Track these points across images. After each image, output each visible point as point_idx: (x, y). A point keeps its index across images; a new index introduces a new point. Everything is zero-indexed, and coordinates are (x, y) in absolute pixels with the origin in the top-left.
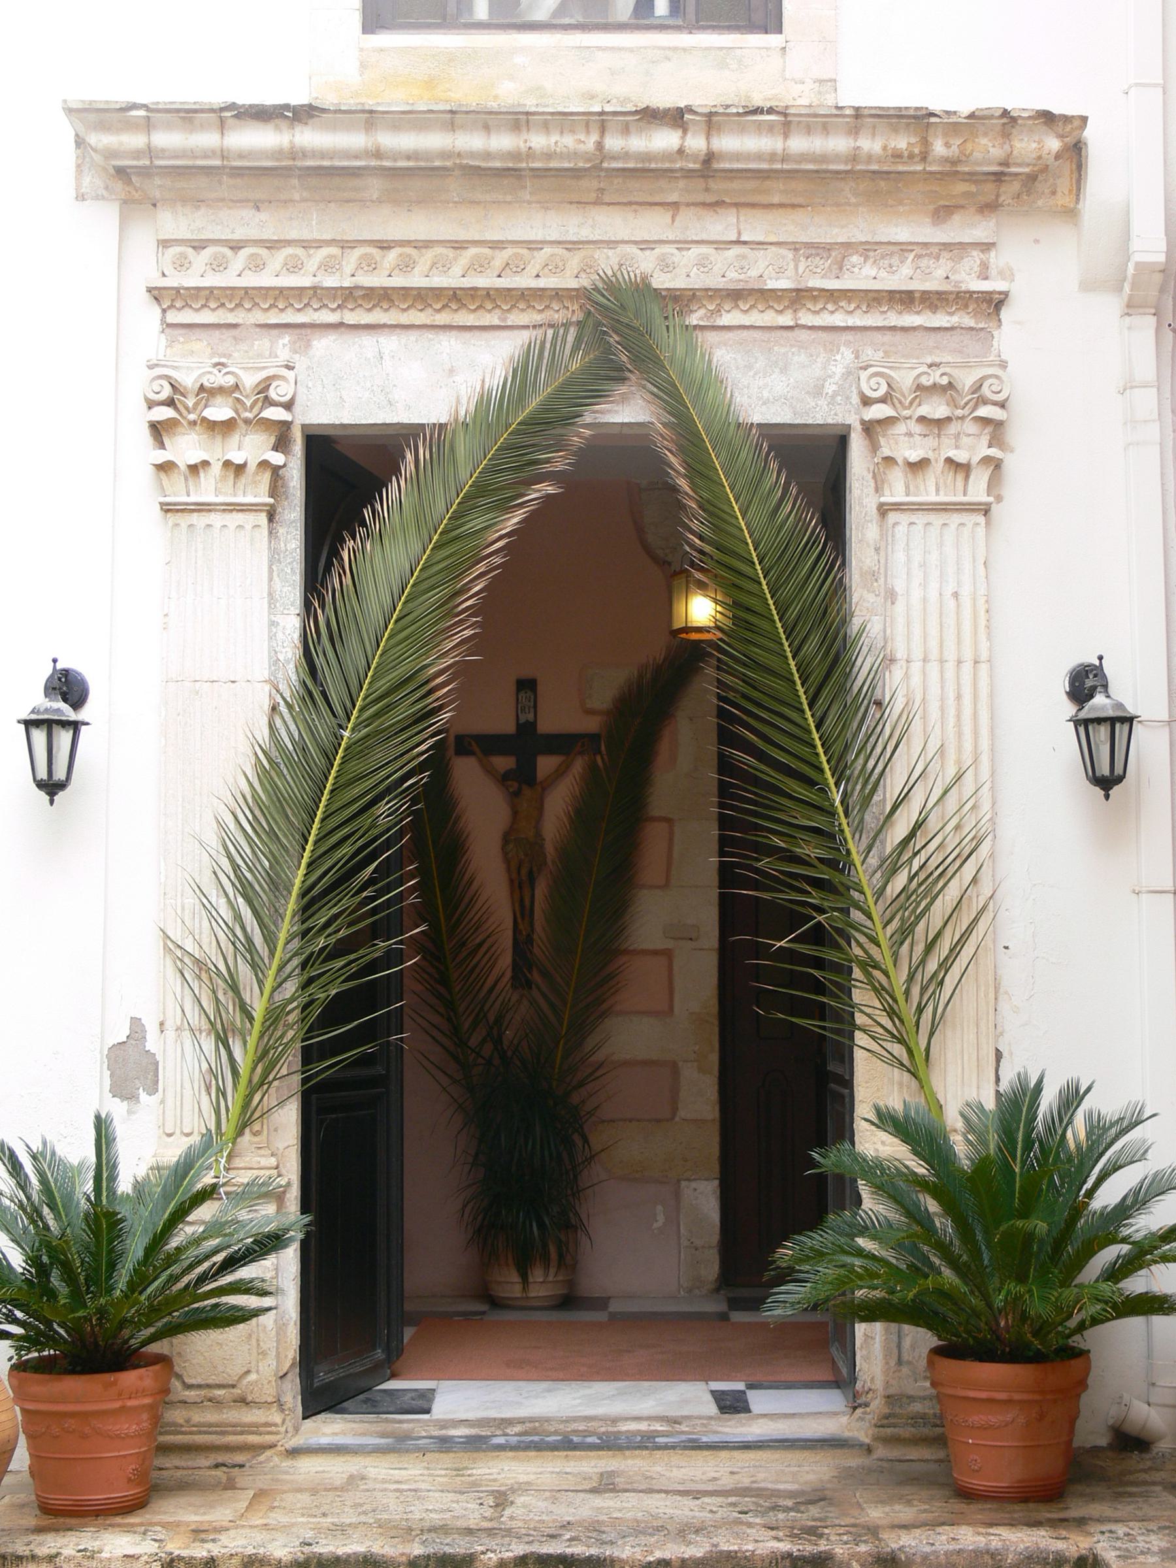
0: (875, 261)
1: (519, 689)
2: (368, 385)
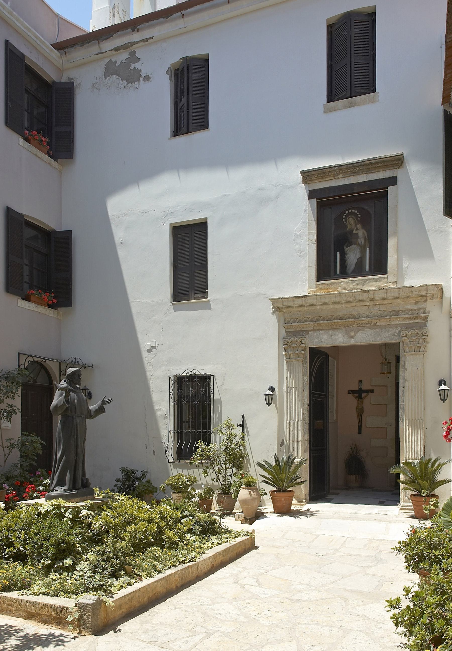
1: (359, 382)
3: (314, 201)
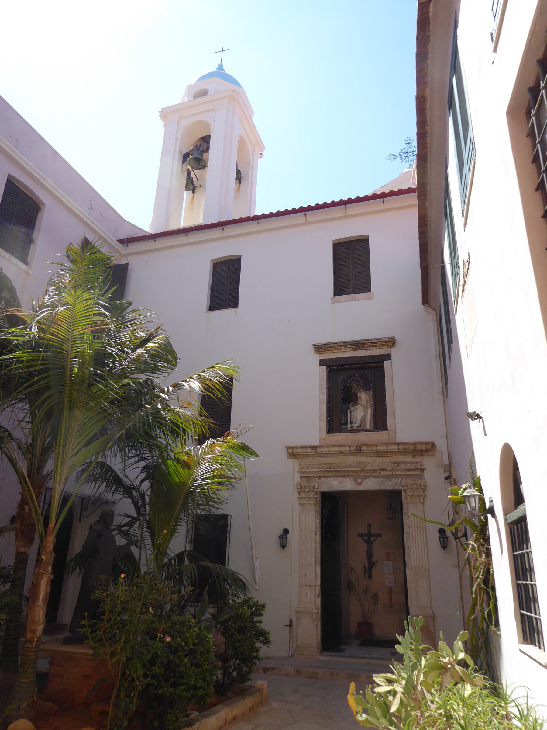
3: (324, 367)
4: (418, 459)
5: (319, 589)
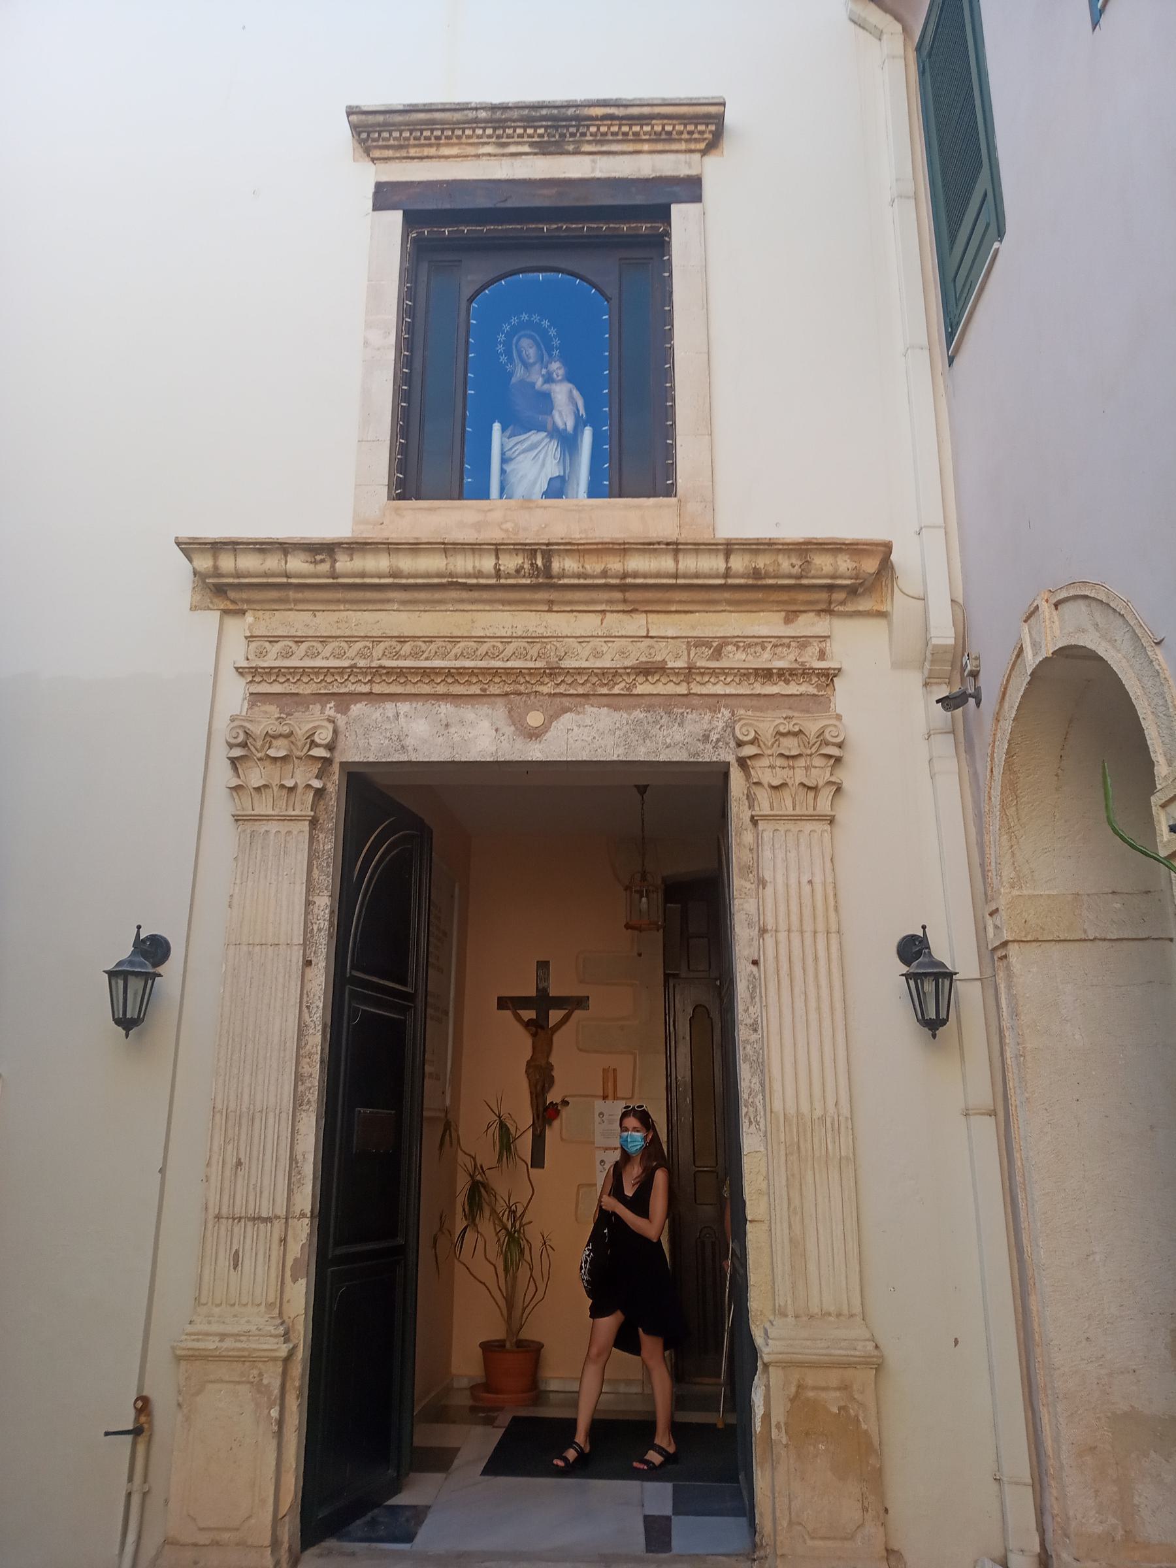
0: (744, 650)
2: (388, 735)
3: (395, 218)
4: (809, 625)
5: (307, 1230)
